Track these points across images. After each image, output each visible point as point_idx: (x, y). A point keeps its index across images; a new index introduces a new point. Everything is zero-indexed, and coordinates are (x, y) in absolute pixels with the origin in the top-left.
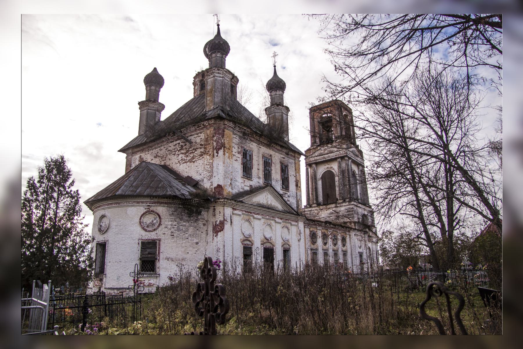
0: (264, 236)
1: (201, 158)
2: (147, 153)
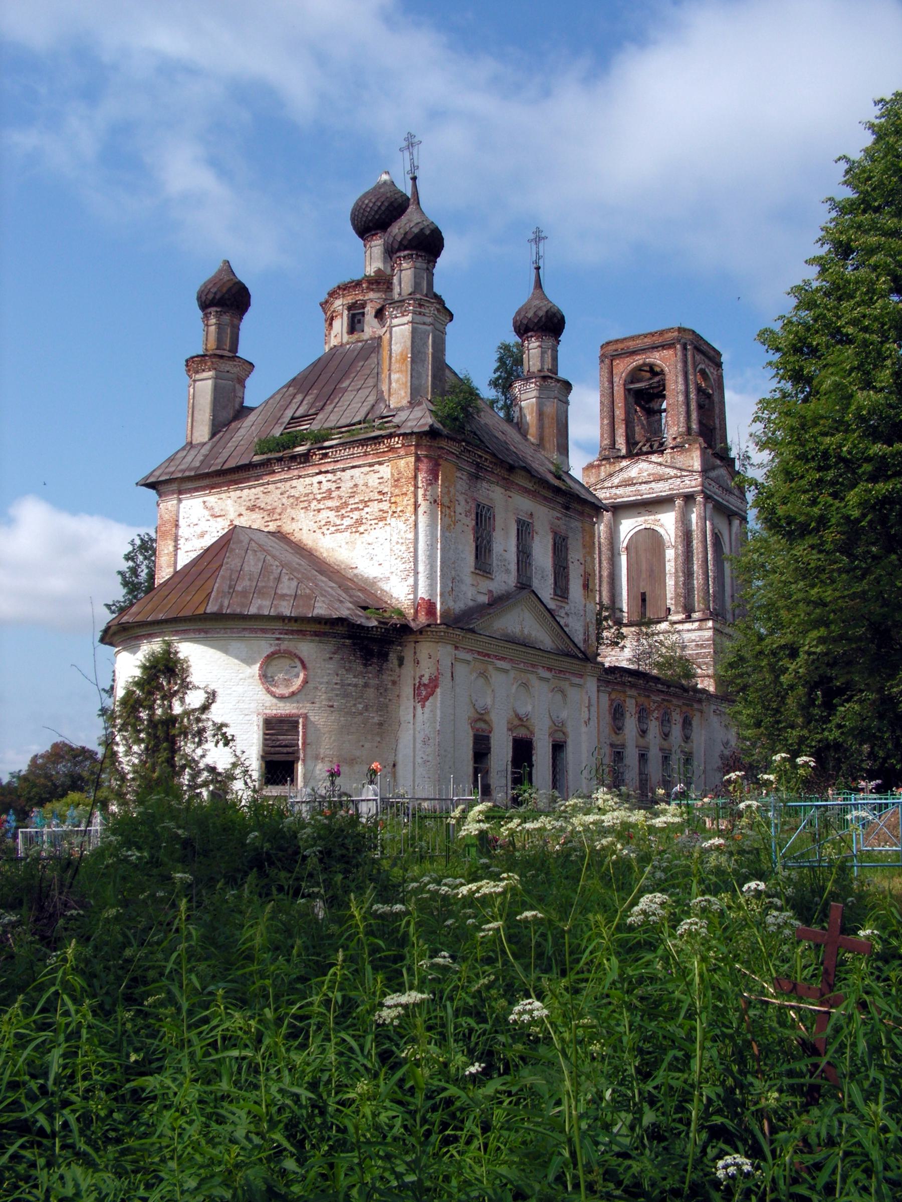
0: (515, 711)
2: (223, 496)
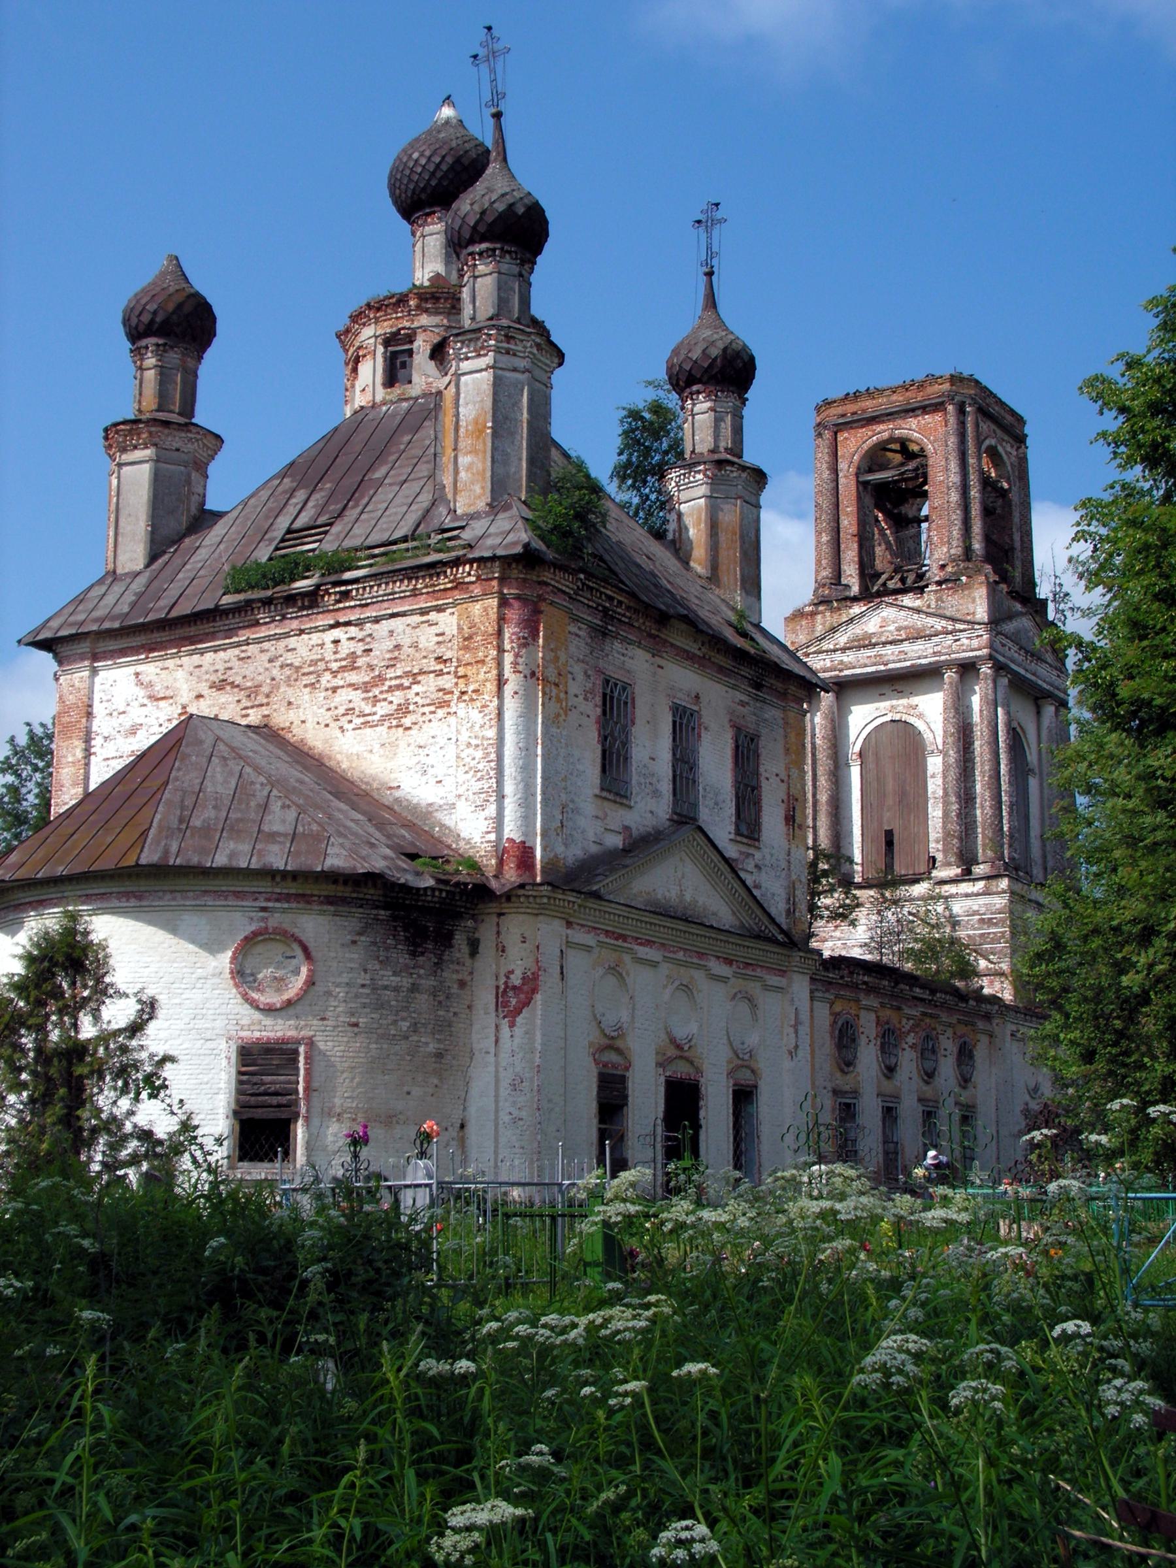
0: (669, 1034)
1: (441, 713)
